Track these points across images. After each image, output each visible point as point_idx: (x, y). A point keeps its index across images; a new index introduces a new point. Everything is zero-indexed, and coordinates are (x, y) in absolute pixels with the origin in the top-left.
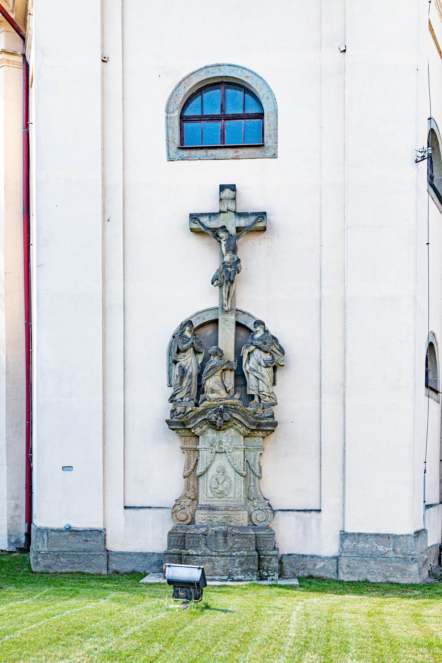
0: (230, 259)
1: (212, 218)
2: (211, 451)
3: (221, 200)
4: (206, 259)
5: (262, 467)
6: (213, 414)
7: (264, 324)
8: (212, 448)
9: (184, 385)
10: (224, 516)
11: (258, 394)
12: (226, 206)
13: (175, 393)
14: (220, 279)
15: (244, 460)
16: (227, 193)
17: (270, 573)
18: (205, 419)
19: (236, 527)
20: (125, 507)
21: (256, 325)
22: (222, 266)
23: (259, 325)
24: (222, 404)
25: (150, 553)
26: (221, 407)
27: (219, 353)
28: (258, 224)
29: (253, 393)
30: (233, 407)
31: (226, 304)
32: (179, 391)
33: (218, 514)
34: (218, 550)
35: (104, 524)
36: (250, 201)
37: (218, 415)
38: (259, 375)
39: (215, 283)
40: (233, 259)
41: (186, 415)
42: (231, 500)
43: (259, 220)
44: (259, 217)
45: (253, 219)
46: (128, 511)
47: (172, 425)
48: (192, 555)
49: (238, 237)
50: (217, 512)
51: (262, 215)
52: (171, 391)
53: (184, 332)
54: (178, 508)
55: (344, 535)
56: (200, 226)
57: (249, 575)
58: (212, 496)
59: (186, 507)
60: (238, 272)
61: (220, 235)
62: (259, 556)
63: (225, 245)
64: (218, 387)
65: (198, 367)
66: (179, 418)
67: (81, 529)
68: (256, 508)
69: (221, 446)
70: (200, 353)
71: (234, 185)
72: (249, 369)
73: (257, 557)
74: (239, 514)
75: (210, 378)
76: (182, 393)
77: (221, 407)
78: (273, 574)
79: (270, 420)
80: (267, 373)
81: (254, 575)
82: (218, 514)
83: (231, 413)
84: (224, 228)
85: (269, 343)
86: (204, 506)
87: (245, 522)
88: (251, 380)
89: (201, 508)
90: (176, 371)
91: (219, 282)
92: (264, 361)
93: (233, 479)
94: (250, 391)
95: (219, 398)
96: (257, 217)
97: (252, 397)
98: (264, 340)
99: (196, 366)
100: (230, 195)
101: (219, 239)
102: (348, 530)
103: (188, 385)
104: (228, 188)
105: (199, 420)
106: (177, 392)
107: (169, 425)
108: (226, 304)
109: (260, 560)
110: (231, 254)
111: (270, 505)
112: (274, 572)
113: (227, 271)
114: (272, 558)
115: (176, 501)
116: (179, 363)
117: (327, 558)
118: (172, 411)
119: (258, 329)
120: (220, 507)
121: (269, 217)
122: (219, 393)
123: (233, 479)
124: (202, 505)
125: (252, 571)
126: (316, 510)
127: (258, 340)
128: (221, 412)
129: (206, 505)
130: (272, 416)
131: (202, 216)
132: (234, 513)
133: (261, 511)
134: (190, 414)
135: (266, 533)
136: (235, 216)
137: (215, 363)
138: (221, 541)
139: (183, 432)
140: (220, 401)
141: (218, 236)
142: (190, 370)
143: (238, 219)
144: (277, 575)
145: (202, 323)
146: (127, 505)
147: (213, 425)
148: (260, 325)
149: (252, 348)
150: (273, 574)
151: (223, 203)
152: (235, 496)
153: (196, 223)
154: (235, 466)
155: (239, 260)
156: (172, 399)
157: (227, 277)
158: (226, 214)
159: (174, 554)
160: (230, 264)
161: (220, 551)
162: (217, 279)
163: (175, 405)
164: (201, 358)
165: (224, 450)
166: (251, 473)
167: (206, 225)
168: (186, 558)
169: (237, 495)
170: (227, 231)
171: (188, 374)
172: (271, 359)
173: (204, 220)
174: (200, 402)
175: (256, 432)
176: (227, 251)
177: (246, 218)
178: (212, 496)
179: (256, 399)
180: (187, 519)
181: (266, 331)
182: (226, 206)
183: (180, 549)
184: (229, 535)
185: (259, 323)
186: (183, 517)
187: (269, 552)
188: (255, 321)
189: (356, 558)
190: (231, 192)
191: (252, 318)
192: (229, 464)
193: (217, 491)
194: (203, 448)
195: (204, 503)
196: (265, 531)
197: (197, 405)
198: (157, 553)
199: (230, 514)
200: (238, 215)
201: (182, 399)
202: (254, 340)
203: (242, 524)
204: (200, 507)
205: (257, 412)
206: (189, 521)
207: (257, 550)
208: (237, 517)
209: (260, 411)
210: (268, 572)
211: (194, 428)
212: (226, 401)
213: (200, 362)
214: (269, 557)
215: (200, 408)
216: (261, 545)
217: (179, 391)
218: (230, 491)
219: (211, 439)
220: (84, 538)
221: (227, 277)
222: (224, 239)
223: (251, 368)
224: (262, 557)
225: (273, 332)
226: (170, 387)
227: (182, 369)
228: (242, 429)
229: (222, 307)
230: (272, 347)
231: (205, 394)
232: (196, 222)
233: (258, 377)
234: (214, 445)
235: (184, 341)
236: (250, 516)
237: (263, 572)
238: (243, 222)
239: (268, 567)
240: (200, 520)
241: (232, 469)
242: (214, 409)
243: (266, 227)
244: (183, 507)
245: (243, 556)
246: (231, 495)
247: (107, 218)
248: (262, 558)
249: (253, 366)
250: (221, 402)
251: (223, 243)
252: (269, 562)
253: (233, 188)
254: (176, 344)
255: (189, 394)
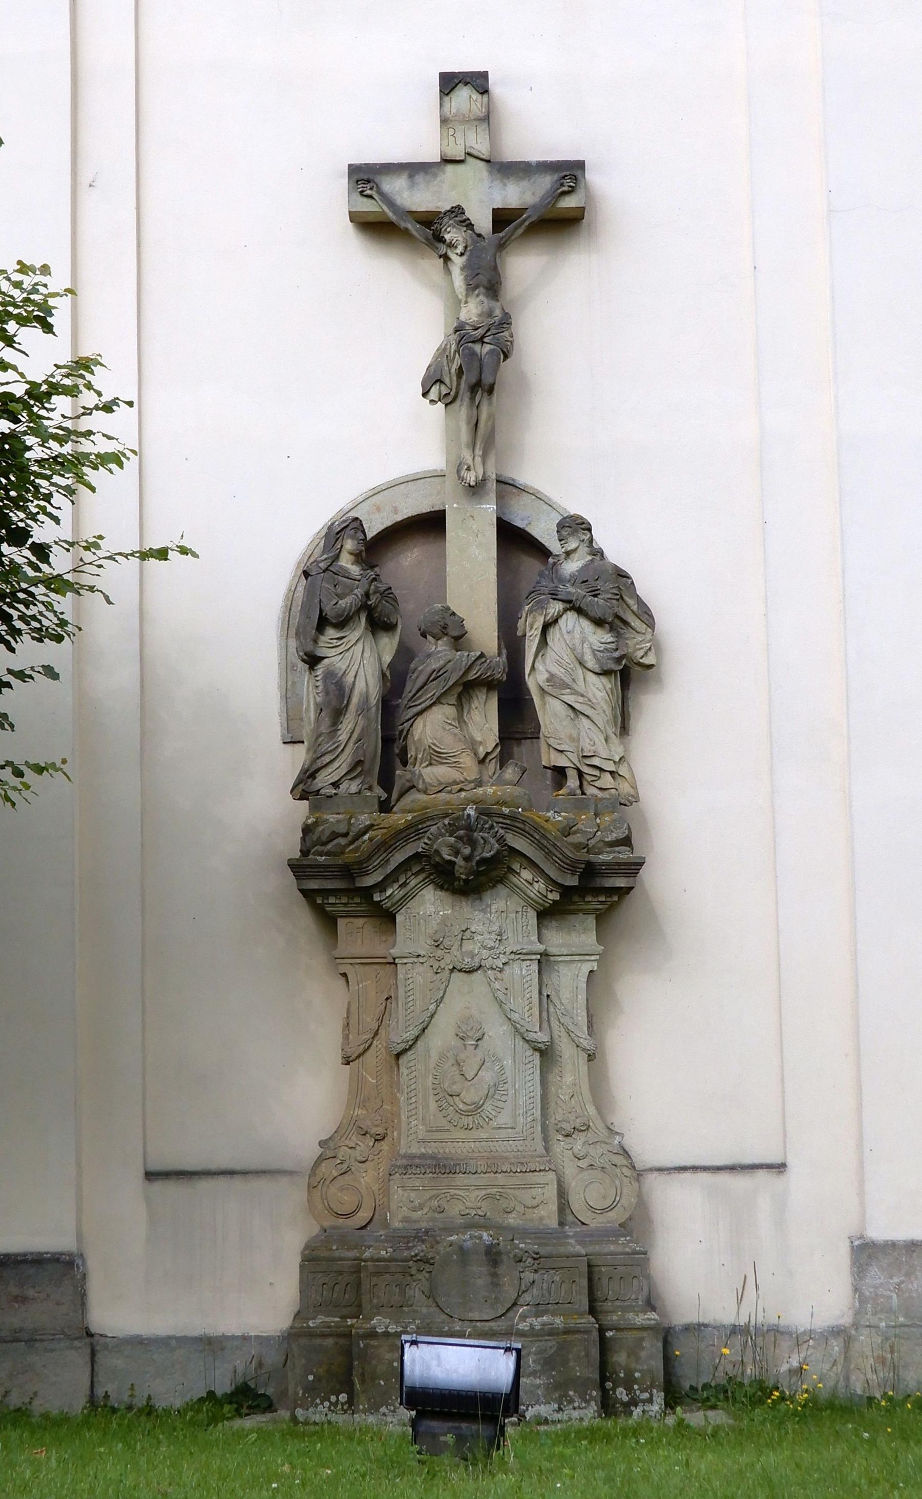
0: (480, 315)
1: (419, 178)
2: (436, 966)
3: (444, 121)
4: (408, 313)
5: (594, 1018)
6: (442, 835)
7: (589, 530)
8: (439, 953)
9: (343, 737)
10: (484, 1192)
11: (578, 765)
12: (460, 141)
13: (315, 767)
14: (447, 381)
15: (540, 993)
16: (464, 96)
17: (638, 1392)
18: (417, 857)
19: (524, 1233)
20: (151, 1176)
21: (564, 533)
22: (456, 337)
23: (574, 533)
24: (468, 801)
25: (233, 1337)
26: (471, 811)
27: (450, 629)
28: (555, 209)
29: (562, 762)
30: (506, 811)
31: (470, 462)
32: (327, 759)
33: (466, 1188)
34: (471, 1316)
35: (79, 1237)
36: (538, 128)
37: (459, 838)
38: (581, 699)
39: (433, 394)
40: (490, 314)
41: (352, 842)
42: (503, 1134)
43: (566, 189)
44: (564, 178)
45: (546, 182)
46: (158, 1186)
47: (310, 877)
48: (386, 1334)
49: (501, 246)
50: (461, 1179)
51: (570, 173)
52: (299, 756)
53: (337, 557)
54: (328, 1169)
55: (866, 1253)
56: (389, 215)
57: (571, 1401)
58: (444, 1123)
59: (355, 1166)
60: (506, 357)
61: (447, 237)
62: (602, 1331)
63: (462, 269)
64: (452, 742)
65: (384, 675)
66: (328, 854)
67: (611, 1119)
68: (583, 1164)
69: (471, 947)
70: (389, 628)
71: (484, 75)
72: (548, 680)
73: (595, 1335)
74: (531, 1186)
75: (425, 715)
76: (336, 764)
77: (471, 811)
78: (646, 1396)
79: (623, 854)
80: (599, 690)
81: (587, 1402)
82: (466, 1188)
83: (501, 831)
84: (457, 211)
85: (607, 592)
86: (417, 1161)
87: (548, 1214)
88: (551, 715)
89: (406, 1167)
90: (310, 691)
91: (444, 391)
92: (593, 651)
93: (508, 1062)
94: (554, 754)
95: (455, 783)
96: (556, 177)
97: (560, 773)
98: (592, 583)
99: (377, 673)
100: (473, 106)
101: (443, 249)
102: (878, 1232)
103: (355, 736)
104: (466, 84)
105: (399, 857)
106: (319, 763)
107: (298, 877)
108: (470, 462)
109: (604, 1346)
110: (482, 297)
111: (626, 1153)
112: (652, 1386)
113: (473, 354)
114: (642, 1339)
115: (322, 1144)
116: (326, 661)
117: (810, 1333)
118: (307, 830)
119: (572, 544)
120: (472, 1162)
121: (591, 176)
122: (455, 765)
123: (508, 1062)
124: (412, 1157)
125: (582, 1387)
126: (769, 1167)
127: (573, 580)
128: (469, 828)
129: (423, 1156)
130: (627, 841)
131: (387, 174)
132: (517, 1179)
133: (598, 1174)
134: (366, 837)
135: (620, 1249)
136: (490, 172)
137: (442, 662)
138: (480, 1282)
139: (344, 900)
140: (461, 790)
141: (442, 240)
142: (360, 686)
143: (497, 184)
144: (659, 1398)
145: (388, 523)
146: (154, 1166)
147: (444, 877)
148: (576, 531)
149: (555, 607)
150: (646, 1396)
151: (451, 132)
152: (515, 1121)
153: (370, 197)
154: (515, 1017)
155: (505, 322)
156: (304, 787)
157: (475, 374)
158: (460, 168)
159: (324, 1336)
160: (481, 332)
161: (476, 1315)
162: (440, 381)
163: (314, 808)
164: (388, 646)
165: (474, 958)
166: (567, 1055)
167: (399, 201)
168: (366, 1346)
169: (521, 1119)
170: (470, 226)
171: (355, 700)
172: (613, 646)
173: (395, 186)
174: (395, 795)
175: (576, 898)
176: (471, 287)
177: (522, 179)
178: (444, 1123)
179: (572, 782)
180: (359, 1207)
181: (598, 553)
182: (460, 141)
183: (344, 1317)
184: (505, 1258)
185: (576, 526)
186: (346, 1201)
187: (631, 1315)
188: (557, 519)
189: (906, 1330)
190: (475, 96)
191: (546, 507)
192: (495, 1007)
193: (461, 1106)
194: (411, 955)
195: (415, 1150)
196: (615, 1243)
197: (385, 807)
198: (257, 1337)
199: (502, 1186)
200: (499, 171)
201: (336, 785)
202: (562, 581)
203: (541, 1219)
204: (404, 1162)
205: (580, 826)
206: (364, 1215)
207: (592, 1311)
208: (526, 1196)
209: (585, 822)
210: (629, 1389)
211: (381, 886)
212: (480, 791)
213: (387, 658)
214: (636, 1334)
215: (399, 818)
216: (608, 1289)
217: (327, 759)
218: (501, 1104)
219: (434, 924)
220: (15, 1291)
221: (475, 374)
222: (460, 249)
223: (551, 678)
224: (609, 1334)
225: (615, 555)
226: (289, 747)
227: (336, 684)
228: (536, 885)
229: (458, 472)
230: (613, 602)
231: (409, 767)
232: (368, 192)
233: (577, 706)
234: (447, 943)
235: (339, 590)
236: (562, 1193)
237: (614, 1389)
238: (513, 195)
239: (629, 1373)
240: (405, 1211)
241: (506, 1027)
242: (446, 821)
243: (583, 208)
244: (345, 1166)
245: (552, 1332)
246: (504, 1119)
247: (85, 177)
248: (611, 1338)
249: (558, 671)
250: (463, 794)
251: (458, 262)
252: (633, 1353)
253: (478, 82)
254: (317, 601)
255: (359, 769)
